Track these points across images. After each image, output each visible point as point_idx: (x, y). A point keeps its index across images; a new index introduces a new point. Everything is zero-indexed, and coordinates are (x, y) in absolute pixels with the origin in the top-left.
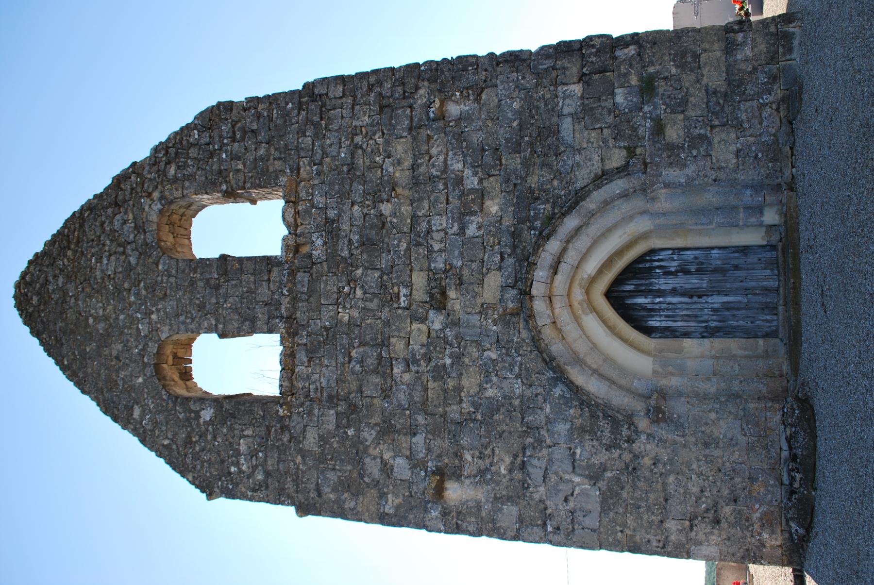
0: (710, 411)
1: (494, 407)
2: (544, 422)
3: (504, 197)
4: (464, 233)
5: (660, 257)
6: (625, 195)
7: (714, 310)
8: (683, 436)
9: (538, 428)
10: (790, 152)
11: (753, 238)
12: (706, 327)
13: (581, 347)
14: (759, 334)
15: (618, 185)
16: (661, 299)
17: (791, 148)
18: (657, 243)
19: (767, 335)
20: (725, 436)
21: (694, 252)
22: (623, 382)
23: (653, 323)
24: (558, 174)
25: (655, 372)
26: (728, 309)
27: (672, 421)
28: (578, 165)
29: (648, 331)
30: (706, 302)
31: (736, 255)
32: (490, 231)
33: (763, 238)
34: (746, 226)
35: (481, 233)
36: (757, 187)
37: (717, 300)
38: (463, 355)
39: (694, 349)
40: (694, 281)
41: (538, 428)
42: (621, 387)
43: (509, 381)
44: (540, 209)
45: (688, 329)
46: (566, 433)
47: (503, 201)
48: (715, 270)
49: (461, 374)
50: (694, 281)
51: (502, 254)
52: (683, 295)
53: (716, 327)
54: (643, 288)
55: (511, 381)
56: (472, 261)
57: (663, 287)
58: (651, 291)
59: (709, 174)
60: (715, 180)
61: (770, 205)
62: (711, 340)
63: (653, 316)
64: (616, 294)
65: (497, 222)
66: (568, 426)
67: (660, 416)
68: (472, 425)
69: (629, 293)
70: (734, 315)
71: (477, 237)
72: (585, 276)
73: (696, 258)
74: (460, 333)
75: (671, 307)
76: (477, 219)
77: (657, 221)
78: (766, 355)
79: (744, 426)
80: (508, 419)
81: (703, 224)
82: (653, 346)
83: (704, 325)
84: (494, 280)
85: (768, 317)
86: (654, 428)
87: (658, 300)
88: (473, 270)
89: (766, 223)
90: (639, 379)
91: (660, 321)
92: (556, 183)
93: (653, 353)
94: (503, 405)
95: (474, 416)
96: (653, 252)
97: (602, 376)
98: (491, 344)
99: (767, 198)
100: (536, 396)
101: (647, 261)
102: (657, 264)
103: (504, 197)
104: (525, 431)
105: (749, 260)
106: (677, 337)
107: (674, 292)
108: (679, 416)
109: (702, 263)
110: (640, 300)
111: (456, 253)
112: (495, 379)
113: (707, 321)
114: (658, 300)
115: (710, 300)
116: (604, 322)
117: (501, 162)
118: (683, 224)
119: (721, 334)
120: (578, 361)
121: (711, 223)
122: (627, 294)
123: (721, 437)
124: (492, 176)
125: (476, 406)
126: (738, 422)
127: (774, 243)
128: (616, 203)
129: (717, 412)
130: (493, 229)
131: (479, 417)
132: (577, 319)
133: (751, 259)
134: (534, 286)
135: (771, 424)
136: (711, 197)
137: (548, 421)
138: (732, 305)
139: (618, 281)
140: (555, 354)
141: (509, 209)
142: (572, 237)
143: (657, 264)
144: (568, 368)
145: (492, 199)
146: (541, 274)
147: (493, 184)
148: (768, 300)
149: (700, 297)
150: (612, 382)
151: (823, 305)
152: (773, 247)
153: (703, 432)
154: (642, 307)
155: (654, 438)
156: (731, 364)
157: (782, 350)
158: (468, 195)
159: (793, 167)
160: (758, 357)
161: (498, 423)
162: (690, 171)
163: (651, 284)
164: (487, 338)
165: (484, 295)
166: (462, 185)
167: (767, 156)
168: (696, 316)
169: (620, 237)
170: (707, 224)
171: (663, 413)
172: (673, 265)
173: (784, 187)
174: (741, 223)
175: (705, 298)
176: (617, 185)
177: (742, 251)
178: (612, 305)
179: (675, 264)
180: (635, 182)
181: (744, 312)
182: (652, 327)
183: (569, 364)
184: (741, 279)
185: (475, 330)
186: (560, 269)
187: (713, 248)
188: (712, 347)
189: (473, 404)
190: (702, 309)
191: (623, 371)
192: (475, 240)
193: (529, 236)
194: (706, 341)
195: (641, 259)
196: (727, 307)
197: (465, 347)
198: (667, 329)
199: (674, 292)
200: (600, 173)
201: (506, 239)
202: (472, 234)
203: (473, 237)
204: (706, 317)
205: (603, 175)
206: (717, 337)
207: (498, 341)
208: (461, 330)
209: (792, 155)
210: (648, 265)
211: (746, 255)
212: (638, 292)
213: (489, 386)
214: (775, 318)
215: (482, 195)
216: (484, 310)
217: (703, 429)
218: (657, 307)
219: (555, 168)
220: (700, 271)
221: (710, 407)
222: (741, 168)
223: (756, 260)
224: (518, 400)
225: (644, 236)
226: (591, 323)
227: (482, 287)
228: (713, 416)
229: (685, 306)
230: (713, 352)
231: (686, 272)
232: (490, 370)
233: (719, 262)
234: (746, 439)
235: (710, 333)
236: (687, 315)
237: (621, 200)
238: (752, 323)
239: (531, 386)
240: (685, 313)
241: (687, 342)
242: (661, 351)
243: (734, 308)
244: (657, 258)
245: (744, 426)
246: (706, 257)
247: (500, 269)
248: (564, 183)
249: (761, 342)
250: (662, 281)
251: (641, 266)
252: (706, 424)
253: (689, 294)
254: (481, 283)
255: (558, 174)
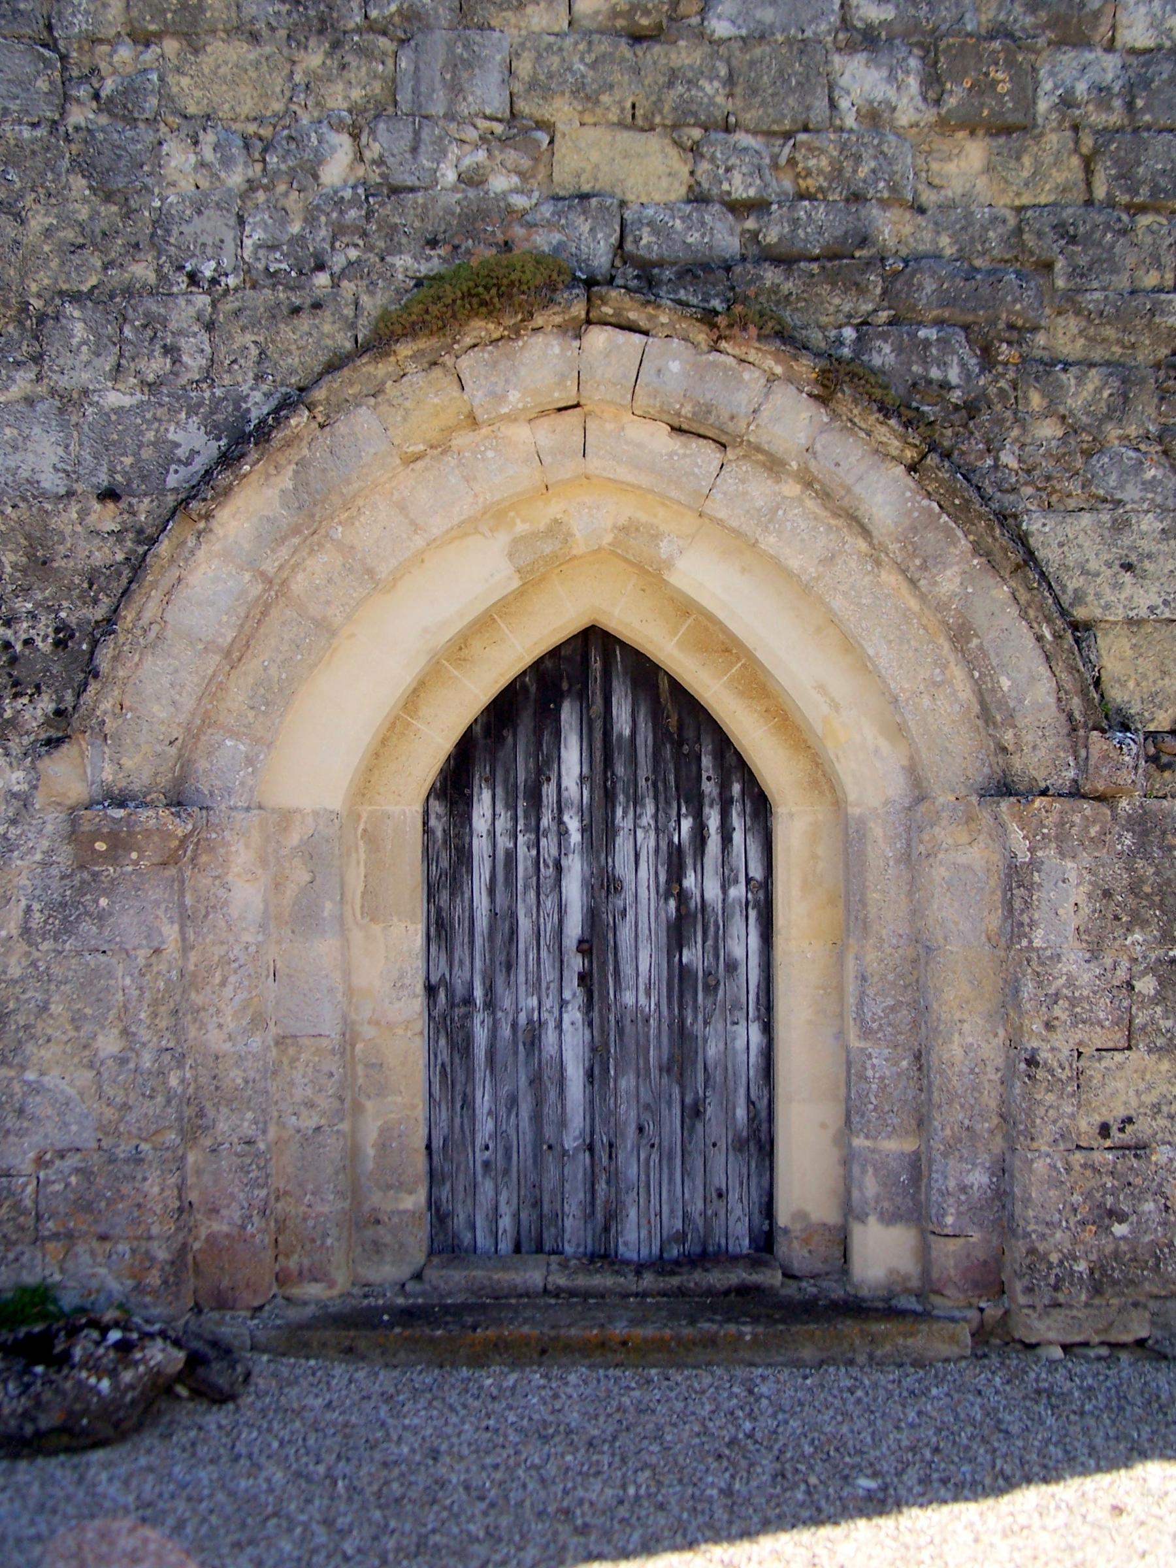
0: (125, 1032)
1: (115, 178)
2: (63, 382)
3: (995, 220)
4: (850, 48)
5: (738, 837)
6: (989, 711)
7: (533, 1036)
8: (26, 931)
9: (37, 359)
10: (1127, 1338)
11: (805, 1179)
12: (469, 1001)
13: (371, 529)
14: (445, 1192)
15: (1033, 686)
16: (575, 837)
17: (1140, 1343)
18: (795, 826)
19: (439, 1214)
20: (35, 1089)
21: (754, 961)
22: (237, 696)
23: (485, 810)
24: (1084, 441)
25: (286, 818)
26: (536, 1081)
27: (82, 889)
28: (1120, 526)
29: (454, 784)
30: (563, 1004)
31: (741, 1113)
32: (858, 159)
33: (802, 1215)
34: (848, 1160)
35: (850, 121)
36: (1002, 1197)
37: (570, 1043)
38: (336, 45)
39: (382, 963)
40: (642, 957)
41: (37, 359)
42: (213, 689)
43: (229, 236)
44: (943, 365)
45: (461, 937)
46: (24, 473)
47: (981, 214)
48: (682, 1037)
49: (255, 38)
50: (642, 957)
51: (758, 206)
52: (592, 917)
53: (469, 1040)
54: (620, 770)
55: (229, 246)
56: (730, 80)
57: (623, 844)
58: (609, 797)
59: (1058, 1039)
60: (1032, 1062)
61: (924, 1253)
62: (421, 1024)
63: (512, 806)
64: (596, 665)
65: (894, 189)
66: (51, 482)
67: (101, 846)
68: (42, 84)
69: (598, 724)
70: (513, 1101)
71: (833, 105)
72: (665, 549)
73: (731, 967)
74: (428, 28)
75: (548, 872)
76: (908, 105)
77: (877, 831)
78: (363, 1223)
79: (73, 1161)
80: (69, 235)
81: (861, 1003)
82: (394, 809)
83: (478, 993)
84: (649, 174)
85: (506, 1222)
86: (54, 821)
87: (573, 824)
88: (691, 83)
89: (857, 1230)
90: (250, 761)
91: (492, 834)
92: (1048, 430)
93: (365, 810)
94: (128, 214)
95: (83, 92)
96: (761, 807)
97: (256, 617)
98: (380, 162)
99: (953, 1245)
100: (167, 350)
101: (724, 787)
102: (713, 821)
103: (995, 220)
104: (25, 306)
105: (718, 1159)
106: (430, 897)
107: (603, 885)
108: (101, 917)
109: (711, 989)
110: (572, 759)
111: (768, 15)
112: (236, 178)
113: (491, 1004)
114: (573, 824)
115: (573, 1015)
116: (485, 624)
117: (1143, 209)
118: (866, 927)
119: (444, 1056)
120: (310, 515)
121: (866, 1032)
122: (598, 707)
123: (31, 1076)
124: (1089, 171)
125: (120, 107)
126: (88, 1138)
127: (782, 1248)
128: (958, 673)
129: (123, 1061)
130: (863, 172)
131: (77, 116)
132: (496, 515)
133: (725, 1168)
134: (622, 337)
135: (86, 1259)
136: (969, 1041)
137: (69, 402)
138: (553, 1095)
139: (646, 674)
140: (341, 428)
141: (944, 240)
142: (825, 495)
143: (713, 821)
144: (285, 481)
145: (989, 169)
146: (675, 366)
147: (1051, 172)
148: (569, 1223)
149: (584, 978)
150: (234, 656)
151: (694, 1112)
152: (765, 1241)
153: (44, 1008)
154: (545, 765)
155: (14, 822)
156: (324, 1103)
157: (387, 1272)
158: (1010, 64)
159: (1066, 1348)
160: (355, 1191)
161: (55, 197)
162: (1073, 964)
163: (637, 801)
164: (405, 144)
165: (590, 134)
166: (1058, 44)
167: (1116, 1255)
168: (509, 966)
169: (821, 688)
170: (861, 1020)
171: (112, 856)
172: (705, 884)
173: (993, 1312)
174: (859, 1142)
175: (580, 999)
176: (1033, 679)
177: (754, 1133)
178: (554, 653)
179: (712, 891)
180: (1040, 754)
181: (527, 1135)
182: (469, 803)
183: (301, 483)
184: (650, 1129)
185: (440, 95)
186: (695, 444)
187: (768, 1028)
188: (390, 1026)
189: (131, 90)
190: (536, 986)
191: (274, 698)
192: (822, 93)
193: (834, 312)
194: (416, 1004)
195: (733, 763)
196: (544, 1080)
197: (365, 52)
198: (463, 856)
199: (603, 885)
200: (1080, 613)
201: (820, 224)
202: (844, 81)
203: (831, 87)
204: (507, 1003)
205: (1075, 626)
206: (432, 1043)
207: (395, 190)
208: (439, 37)
209: (1114, 1346)
210: (709, 788)
211: (740, 1145)
212: (604, 751)
213: (209, 155)
214: (505, 1245)
215: (1009, 129)
216: (518, 129)
217: (56, 1008)
218: (545, 822)
219: (1112, 432)
220: (681, 980)
221: (144, 1035)
222: (1078, 1157)
223: (719, 1180)
224: (152, 278)
225: (822, 779)
226: (477, 573)
227: (621, 125)
228: (109, 1044)
229: (548, 927)
230: (369, 1032)
231: (677, 935)
232: (272, 159)
233: (713, 1050)
234: (27, 1167)
235: (448, 1015)
236: (513, 932)
237: (966, 693)
238: (487, 1164)
239: (210, 327)
240: (525, 925)
241: (408, 934)
242: (372, 839)
243: (539, 1103)
244: (736, 821)
245: (73, 1161)
246: (736, 1006)
247: (698, 198)
248: (1048, 465)
249: (414, 1200)
250: (647, 842)
251: (707, 761)
252: (77, 1021)
253: (597, 941)
254: (635, 122)
255: (1084, 441)
